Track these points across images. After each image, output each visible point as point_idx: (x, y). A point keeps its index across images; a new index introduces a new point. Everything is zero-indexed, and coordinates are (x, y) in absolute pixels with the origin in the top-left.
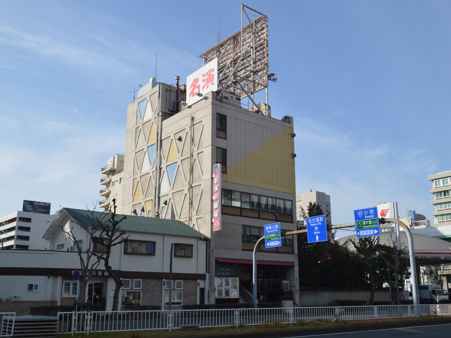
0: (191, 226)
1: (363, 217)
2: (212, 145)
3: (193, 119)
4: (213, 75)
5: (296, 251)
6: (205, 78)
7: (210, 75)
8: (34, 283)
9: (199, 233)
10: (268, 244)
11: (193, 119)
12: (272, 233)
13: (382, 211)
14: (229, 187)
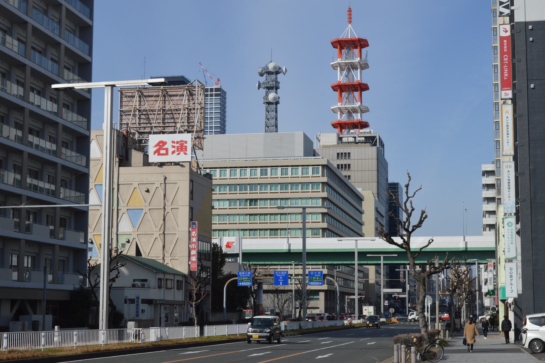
0: (165, 264)
1: (314, 275)
2: (189, 206)
3: (165, 178)
4: (186, 147)
6: (176, 145)
9: (173, 269)
10: (240, 284)
11: (165, 178)
12: (244, 277)
13: (228, 243)
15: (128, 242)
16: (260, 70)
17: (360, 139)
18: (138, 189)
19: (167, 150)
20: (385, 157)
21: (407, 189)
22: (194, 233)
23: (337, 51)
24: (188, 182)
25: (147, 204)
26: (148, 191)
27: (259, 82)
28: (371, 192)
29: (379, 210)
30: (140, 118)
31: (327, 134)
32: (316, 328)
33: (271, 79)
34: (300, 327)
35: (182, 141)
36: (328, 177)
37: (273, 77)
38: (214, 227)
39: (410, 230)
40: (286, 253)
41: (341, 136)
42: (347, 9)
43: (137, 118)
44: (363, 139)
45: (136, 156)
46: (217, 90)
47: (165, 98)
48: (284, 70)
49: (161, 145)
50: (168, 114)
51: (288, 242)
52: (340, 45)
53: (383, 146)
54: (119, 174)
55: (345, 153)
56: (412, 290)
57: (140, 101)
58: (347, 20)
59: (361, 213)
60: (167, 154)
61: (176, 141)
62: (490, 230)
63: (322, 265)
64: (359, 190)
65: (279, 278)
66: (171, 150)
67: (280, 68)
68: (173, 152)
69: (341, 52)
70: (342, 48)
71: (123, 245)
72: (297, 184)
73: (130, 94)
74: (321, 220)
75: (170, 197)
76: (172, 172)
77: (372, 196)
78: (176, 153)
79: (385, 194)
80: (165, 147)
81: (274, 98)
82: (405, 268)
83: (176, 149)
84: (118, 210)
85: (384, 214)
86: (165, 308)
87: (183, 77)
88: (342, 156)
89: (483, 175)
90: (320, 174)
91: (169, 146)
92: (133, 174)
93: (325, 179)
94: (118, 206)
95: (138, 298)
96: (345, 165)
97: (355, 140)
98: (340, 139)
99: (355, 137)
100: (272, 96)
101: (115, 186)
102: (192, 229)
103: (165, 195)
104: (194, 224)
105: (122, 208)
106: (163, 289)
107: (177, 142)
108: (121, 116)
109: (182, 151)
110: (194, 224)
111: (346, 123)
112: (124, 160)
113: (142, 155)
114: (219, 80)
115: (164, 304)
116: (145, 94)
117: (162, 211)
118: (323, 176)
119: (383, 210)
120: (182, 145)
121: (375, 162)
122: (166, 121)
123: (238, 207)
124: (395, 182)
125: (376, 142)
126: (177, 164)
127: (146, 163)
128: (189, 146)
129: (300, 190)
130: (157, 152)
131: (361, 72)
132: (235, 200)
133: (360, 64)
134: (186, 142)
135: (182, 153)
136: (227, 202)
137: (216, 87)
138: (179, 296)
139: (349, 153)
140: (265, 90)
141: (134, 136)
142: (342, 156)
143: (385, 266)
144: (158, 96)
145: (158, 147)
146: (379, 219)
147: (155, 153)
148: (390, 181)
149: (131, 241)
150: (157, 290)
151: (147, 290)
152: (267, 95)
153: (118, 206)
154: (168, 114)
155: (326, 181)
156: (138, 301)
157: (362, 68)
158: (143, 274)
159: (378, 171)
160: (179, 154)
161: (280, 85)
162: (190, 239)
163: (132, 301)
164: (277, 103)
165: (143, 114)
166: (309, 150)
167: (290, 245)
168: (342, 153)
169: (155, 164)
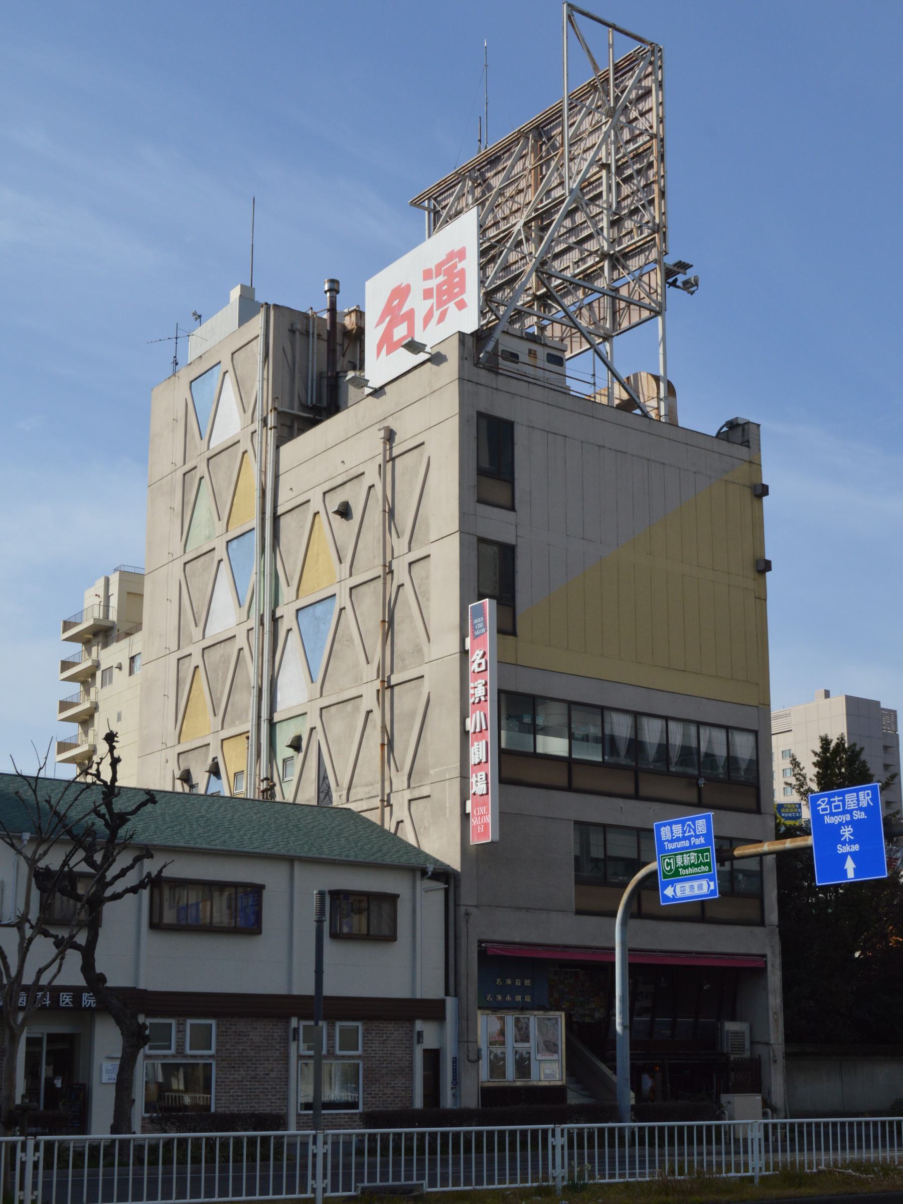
3: (390, 436)
4: (463, 271)
6: (433, 283)
7: (450, 273)
9: (418, 852)
10: (669, 892)
11: (390, 436)
12: (682, 851)
14: (526, 685)
102: (475, 637)
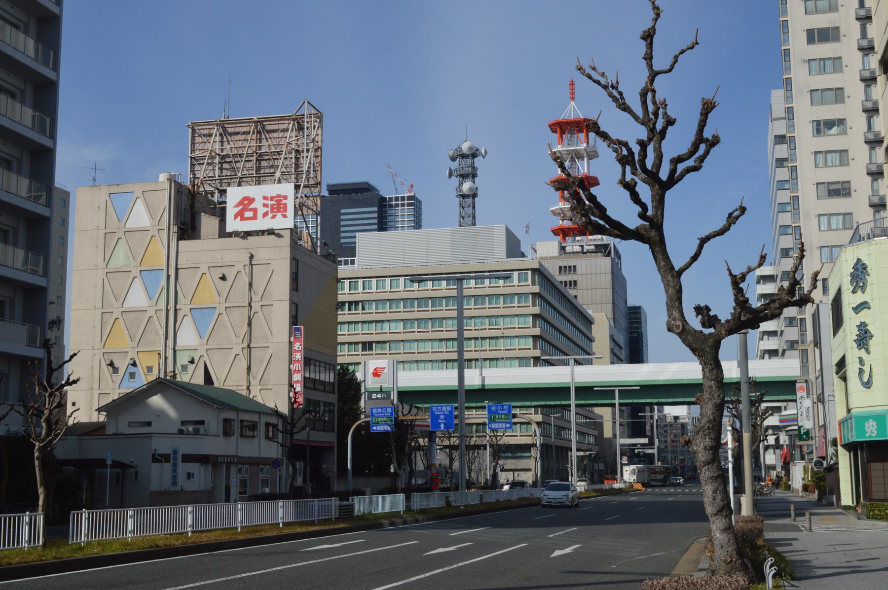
0: (251, 397)
2: (290, 300)
3: (252, 257)
4: (285, 205)
5: (336, 430)
6: (269, 203)
7: (279, 202)
8: (192, 471)
9: (264, 406)
10: (375, 428)
11: (252, 257)
12: (381, 417)
14: (313, 356)
15: (192, 362)
16: (451, 153)
17: (588, 247)
18: (208, 275)
19: (255, 211)
20: (623, 271)
21: (650, 46)
22: (298, 346)
23: (556, 136)
24: (288, 261)
25: (223, 299)
26: (223, 278)
27: (450, 169)
28: (603, 314)
29: (615, 338)
30: (221, 169)
31: (546, 243)
32: (487, 504)
33: (466, 165)
34: (448, 504)
35: (279, 196)
36: (541, 287)
37: (469, 161)
38: (340, 339)
39: (664, 175)
40: (478, 390)
41: (564, 245)
42: (569, 82)
43: (217, 168)
44: (593, 247)
45: (208, 223)
46: (409, 198)
47: (261, 136)
48: (483, 152)
49: (245, 203)
50: (266, 160)
51: (481, 374)
52: (561, 129)
53: (619, 258)
54: (177, 252)
55: (570, 267)
56: (662, 447)
57: (222, 142)
58: (569, 96)
59: (591, 340)
60: (255, 217)
61: (269, 196)
62: (770, 358)
63: (535, 407)
64: (590, 312)
65: (438, 417)
66: (261, 210)
67: (477, 150)
68: (265, 215)
69: (562, 137)
70: (562, 133)
71: (184, 368)
72: (497, 296)
73: (206, 132)
74: (531, 346)
75: (259, 286)
76: (264, 248)
77: (605, 319)
78: (270, 215)
79: (623, 322)
80: (252, 206)
81: (470, 189)
82: (652, 410)
83: (269, 209)
84: (176, 310)
85: (622, 345)
86: (239, 471)
87: (367, 183)
88: (565, 271)
89: (758, 282)
90: (530, 282)
91: (258, 204)
92: (203, 251)
93: (536, 289)
94: (176, 303)
95: (175, 452)
96: (570, 282)
97: (583, 250)
98: (563, 248)
99: (582, 246)
100: (467, 186)
101: (172, 272)
102: (295, 338)
103: (251, 285)
104: (299, 330)
105: (183, 307)
106: (234, 438)
107: (272, 198)
108: (193, 165)
109: (279, 211)
110: (299, 330)
111: (570, 229)
112: (187, 228)
113: (217, 221)
114: (412, 186)
115: (237, 464)
116: (230, 130)
117: (246, 310)
118: (533, 284)
119: (621, 339)
120: (279, 203)
121: (609, 276)
122: (262, 171)
123: (416, 330)
124: (636, 305)
125: (610, 251)
126: (271, 232)
127: (223, 233)
128: (290, 203)
129: (501, 305)
130: (240, 215)
131: (588, 163)
132: (412, 320)
133: (587, 153)
134: (285, 197)
135: (279, 215)
136: (401, 324)
137: (409, 194)
138: (272, 451)
139: (575, 267)
140: (458, 179)
141: (213, 196)
142: (565, 271)
143: (624, 408)
144: (248, 133)
145: (241, 207)
146: (615, 351)
147: (236, 217)
148: (631, 303)
149: (196, 361)
150: (221, 440)
151: (193, 439)
152: (461, 184)
153: (176, 303)
154: (266, 160)
155: (538, 291)
156: (175, 458)
157: (590, 158)
158: (196, 412)
159: (613, 288)
160: (274, 217)
161: (478, 172)
162: (290, 354)
163: (166, 458)
164: (474, 196)
165: (226, 162)
166: (514, 248)
167: (483, 379)
168: (565, 267)
169: (236, 234)
